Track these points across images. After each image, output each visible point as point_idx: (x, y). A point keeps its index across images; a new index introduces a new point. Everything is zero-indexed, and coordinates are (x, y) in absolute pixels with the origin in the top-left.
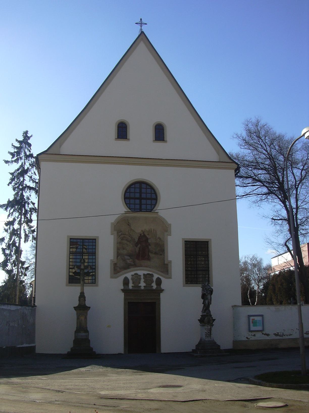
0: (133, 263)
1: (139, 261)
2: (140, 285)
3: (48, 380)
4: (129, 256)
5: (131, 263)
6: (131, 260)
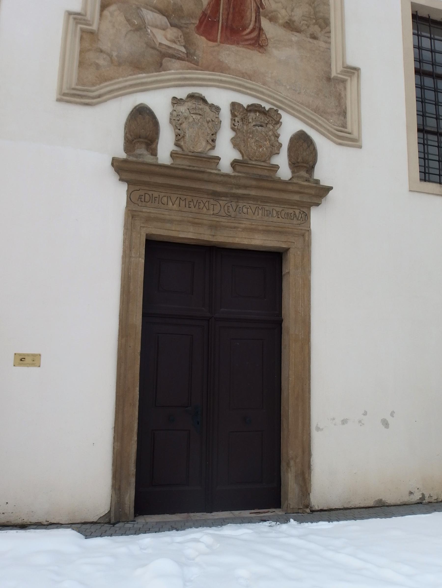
0: (185, 47)
1: (211, 44)
2: (214, 153)
3: (228, 217)
4: (162, 12)
5: (174, 46)
6: (172, 33)
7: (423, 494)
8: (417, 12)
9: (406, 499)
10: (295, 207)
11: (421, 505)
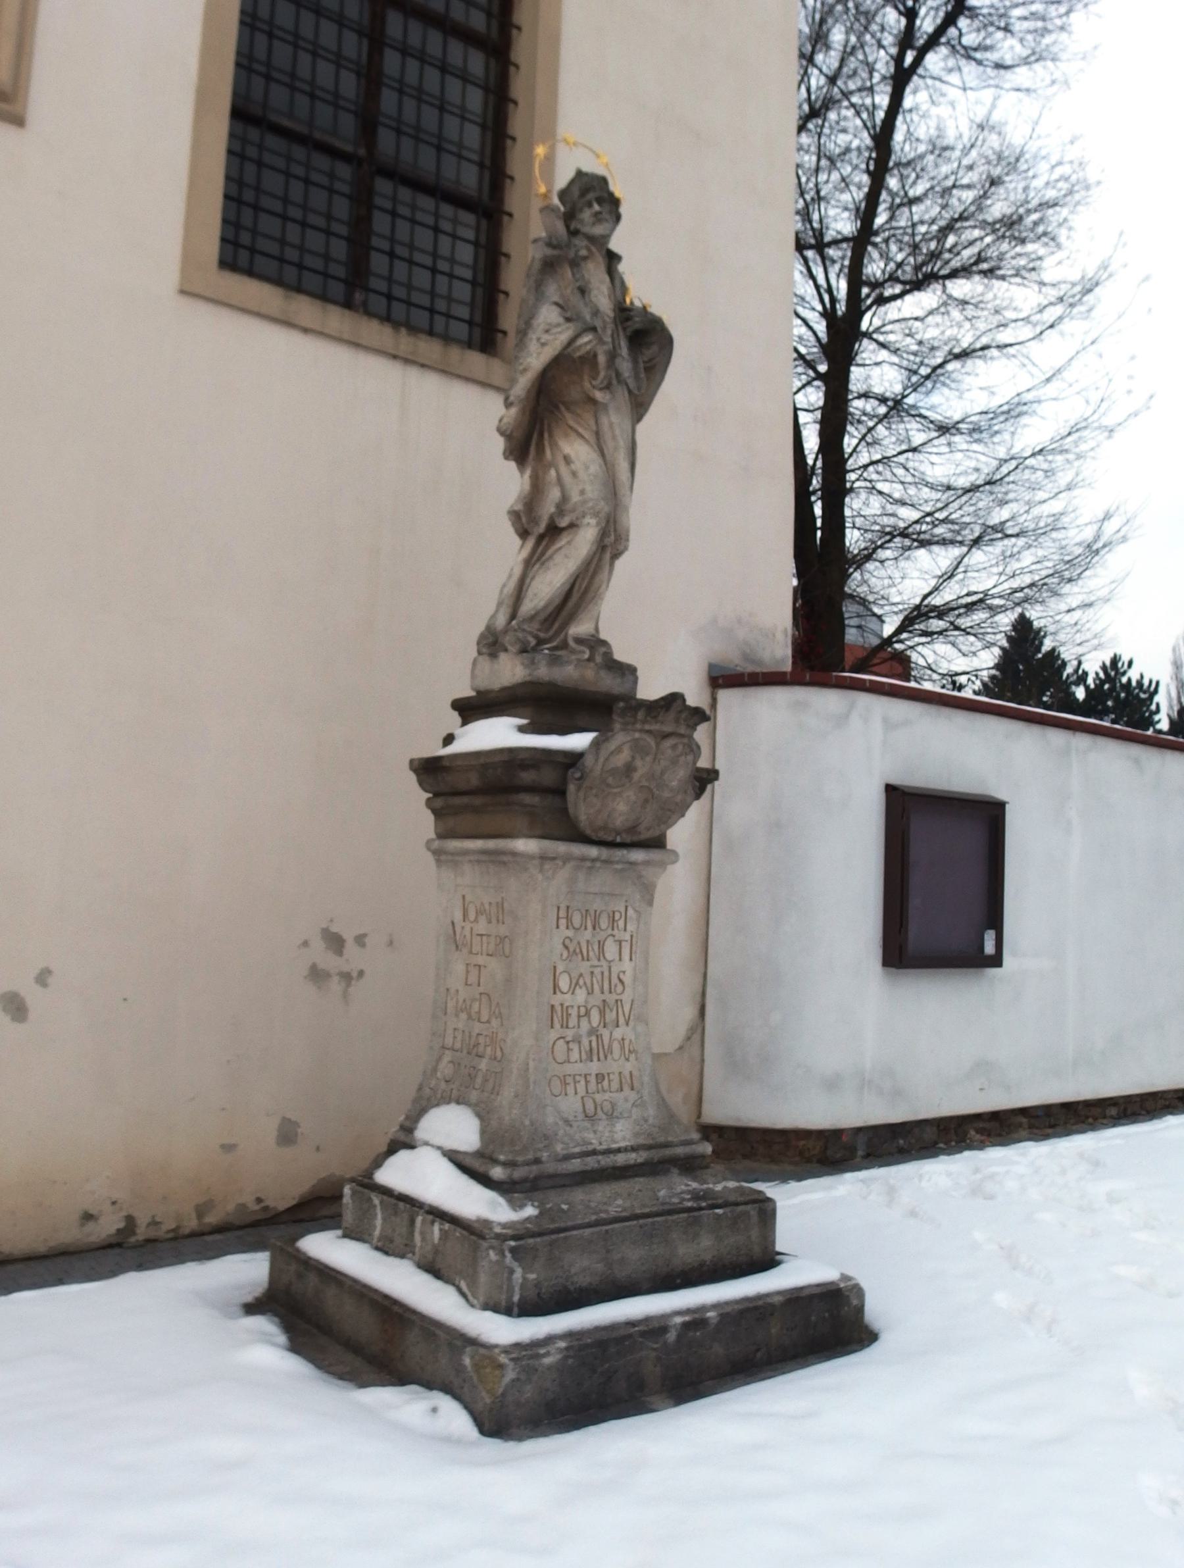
7: (130, 1220)
8: (305, 977)
9: (70, 1234)
10: (640, 1160)
11: (117, 1251)
